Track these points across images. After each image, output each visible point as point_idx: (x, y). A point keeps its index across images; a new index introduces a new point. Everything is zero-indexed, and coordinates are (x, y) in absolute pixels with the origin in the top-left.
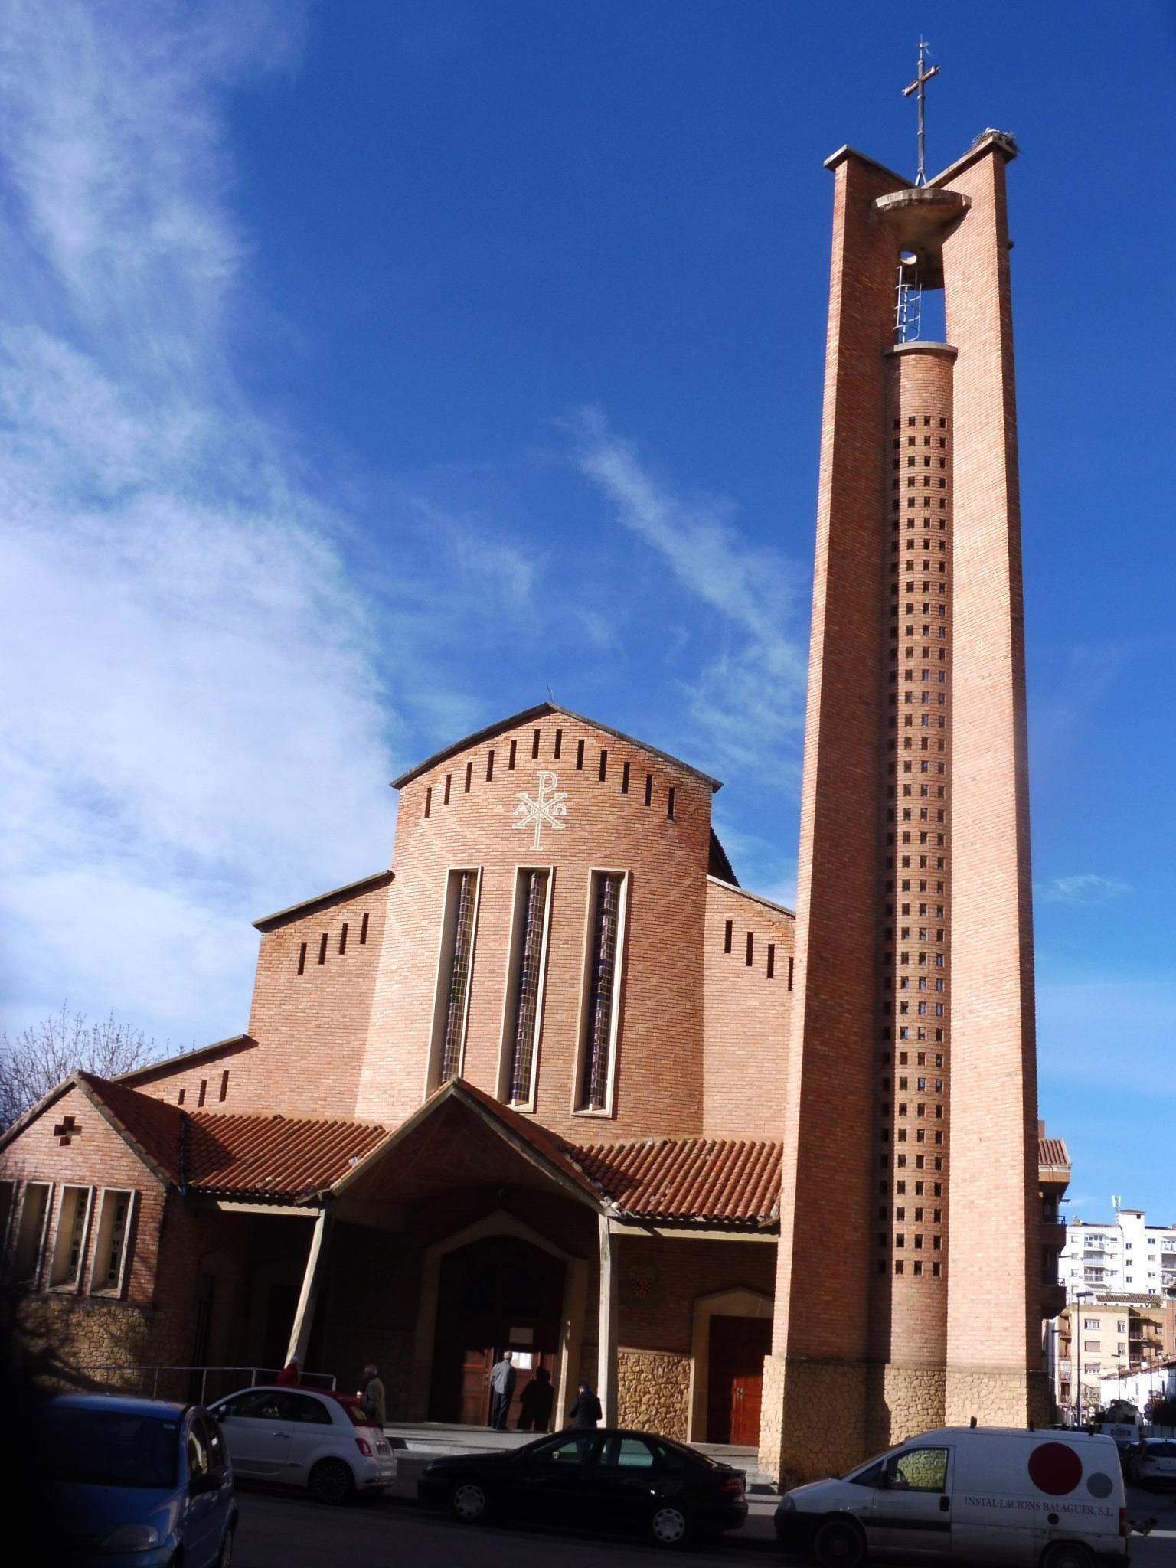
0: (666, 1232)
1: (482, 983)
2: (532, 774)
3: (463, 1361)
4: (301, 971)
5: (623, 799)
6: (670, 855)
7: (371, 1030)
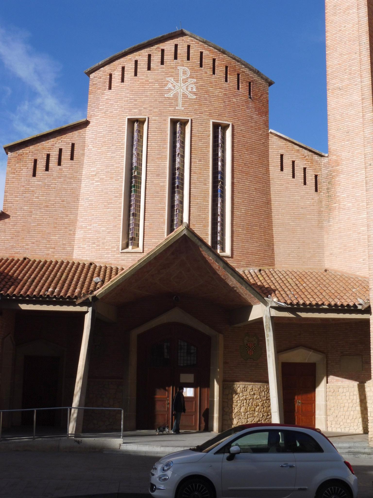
0: (303, 315)
1: (152, 182)
2: (175, 68)
3: (154, 394)
4: (34, 175)
5: (226, 85)
6: (251, 117)
7: (81, 209)
